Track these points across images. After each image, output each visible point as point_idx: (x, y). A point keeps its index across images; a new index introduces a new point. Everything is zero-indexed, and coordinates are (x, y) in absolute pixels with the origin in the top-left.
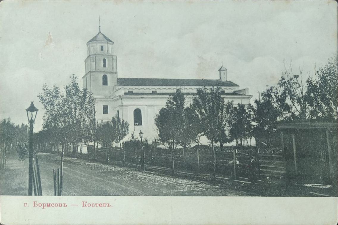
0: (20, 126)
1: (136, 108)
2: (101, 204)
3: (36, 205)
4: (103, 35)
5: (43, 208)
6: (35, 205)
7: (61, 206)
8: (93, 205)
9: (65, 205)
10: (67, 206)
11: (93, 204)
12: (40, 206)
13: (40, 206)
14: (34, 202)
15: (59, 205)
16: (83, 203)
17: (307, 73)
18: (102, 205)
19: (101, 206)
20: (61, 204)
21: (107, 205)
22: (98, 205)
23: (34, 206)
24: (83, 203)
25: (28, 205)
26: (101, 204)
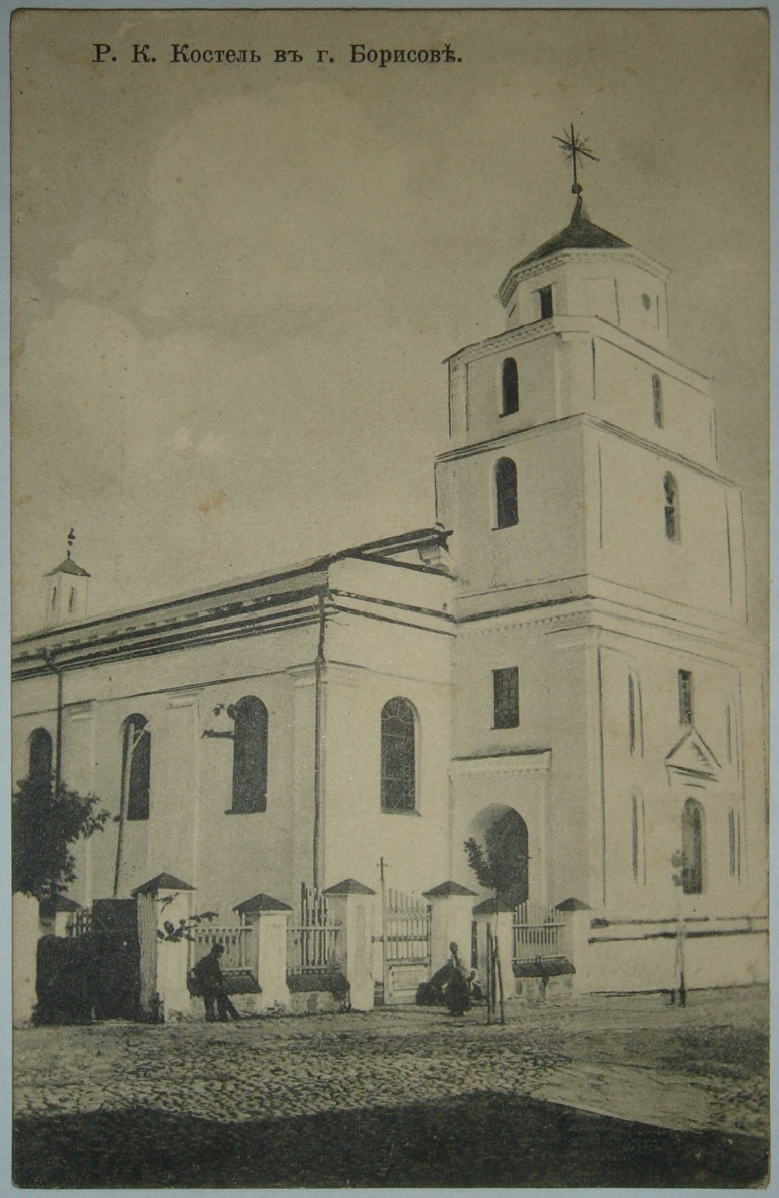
0: (73, 838)
1: (136, 712)
2: (231, 53)
3: (358, 57)
4: (659, 991)
5: (383, 66)
6: (357, 56)
7: (436, 59)
8: (208, 57)
9: (295, 56)
10: (301, 58)
11: (208, 54)
12: (196, 54)
13: (196, 54)
14: (354, 47)
15: (406, 58)
16: (176, 49)
17: (327, 907)
18: (234, 54)
19: (231, 58)
20: (399, 59)
21: (290, 57)
22: (222, 53)
23: (354, 60)
24: (176, 49)
25: (330, 56)
26: (231, 53)
